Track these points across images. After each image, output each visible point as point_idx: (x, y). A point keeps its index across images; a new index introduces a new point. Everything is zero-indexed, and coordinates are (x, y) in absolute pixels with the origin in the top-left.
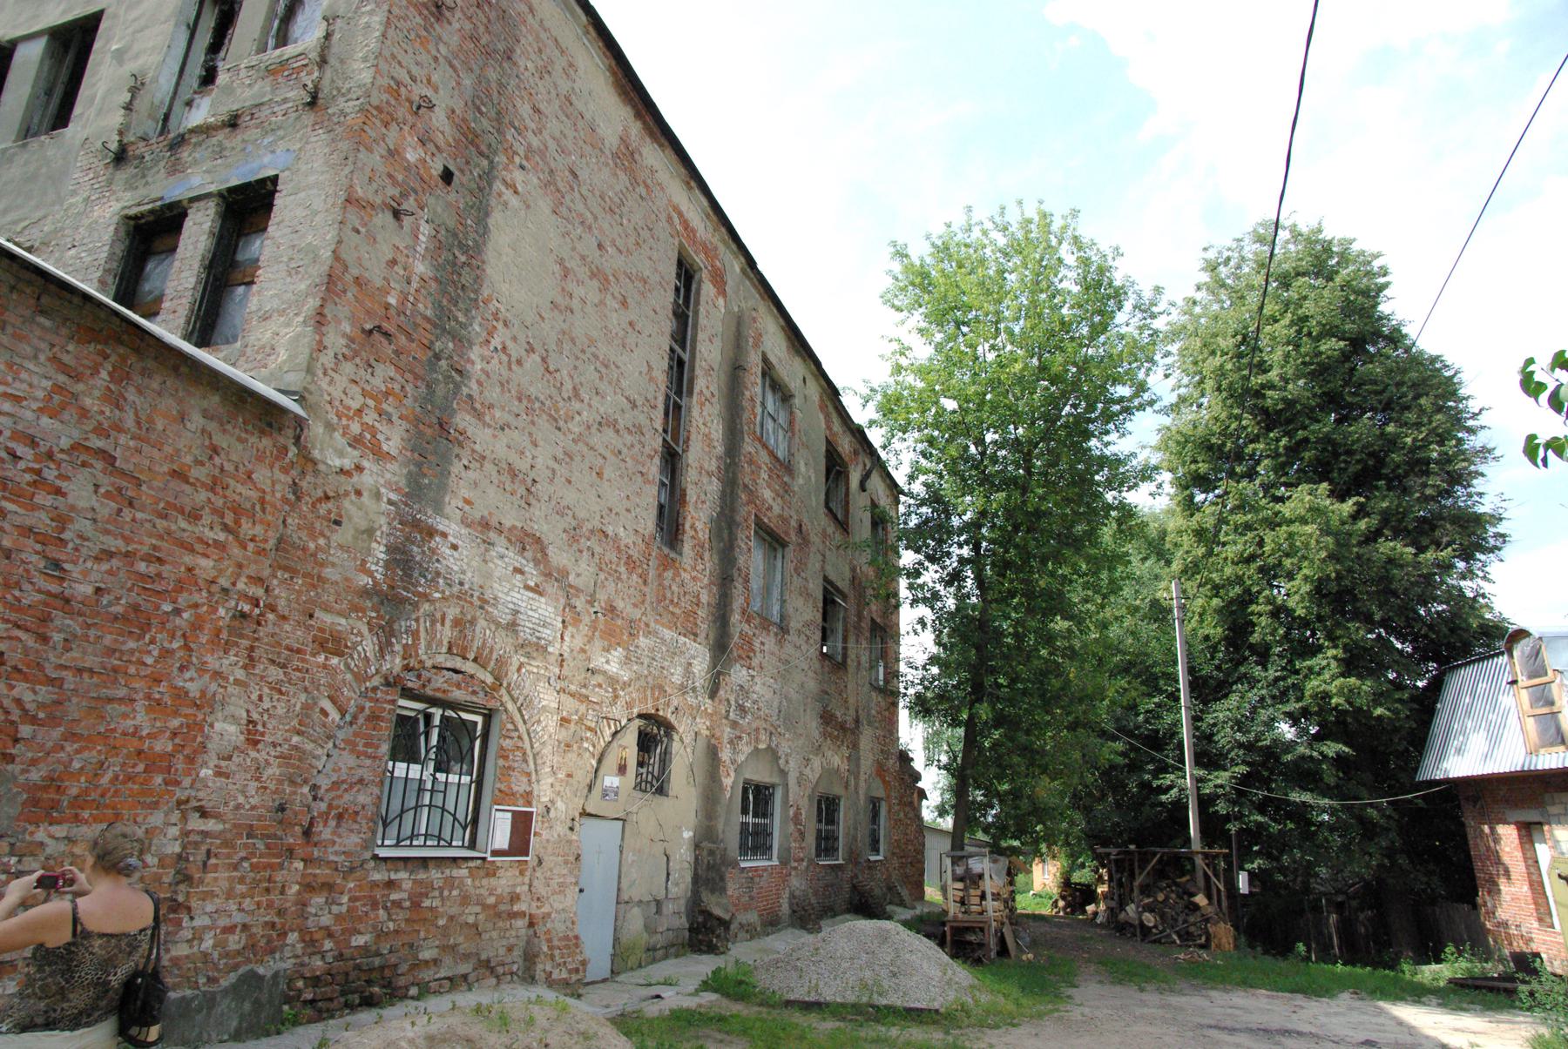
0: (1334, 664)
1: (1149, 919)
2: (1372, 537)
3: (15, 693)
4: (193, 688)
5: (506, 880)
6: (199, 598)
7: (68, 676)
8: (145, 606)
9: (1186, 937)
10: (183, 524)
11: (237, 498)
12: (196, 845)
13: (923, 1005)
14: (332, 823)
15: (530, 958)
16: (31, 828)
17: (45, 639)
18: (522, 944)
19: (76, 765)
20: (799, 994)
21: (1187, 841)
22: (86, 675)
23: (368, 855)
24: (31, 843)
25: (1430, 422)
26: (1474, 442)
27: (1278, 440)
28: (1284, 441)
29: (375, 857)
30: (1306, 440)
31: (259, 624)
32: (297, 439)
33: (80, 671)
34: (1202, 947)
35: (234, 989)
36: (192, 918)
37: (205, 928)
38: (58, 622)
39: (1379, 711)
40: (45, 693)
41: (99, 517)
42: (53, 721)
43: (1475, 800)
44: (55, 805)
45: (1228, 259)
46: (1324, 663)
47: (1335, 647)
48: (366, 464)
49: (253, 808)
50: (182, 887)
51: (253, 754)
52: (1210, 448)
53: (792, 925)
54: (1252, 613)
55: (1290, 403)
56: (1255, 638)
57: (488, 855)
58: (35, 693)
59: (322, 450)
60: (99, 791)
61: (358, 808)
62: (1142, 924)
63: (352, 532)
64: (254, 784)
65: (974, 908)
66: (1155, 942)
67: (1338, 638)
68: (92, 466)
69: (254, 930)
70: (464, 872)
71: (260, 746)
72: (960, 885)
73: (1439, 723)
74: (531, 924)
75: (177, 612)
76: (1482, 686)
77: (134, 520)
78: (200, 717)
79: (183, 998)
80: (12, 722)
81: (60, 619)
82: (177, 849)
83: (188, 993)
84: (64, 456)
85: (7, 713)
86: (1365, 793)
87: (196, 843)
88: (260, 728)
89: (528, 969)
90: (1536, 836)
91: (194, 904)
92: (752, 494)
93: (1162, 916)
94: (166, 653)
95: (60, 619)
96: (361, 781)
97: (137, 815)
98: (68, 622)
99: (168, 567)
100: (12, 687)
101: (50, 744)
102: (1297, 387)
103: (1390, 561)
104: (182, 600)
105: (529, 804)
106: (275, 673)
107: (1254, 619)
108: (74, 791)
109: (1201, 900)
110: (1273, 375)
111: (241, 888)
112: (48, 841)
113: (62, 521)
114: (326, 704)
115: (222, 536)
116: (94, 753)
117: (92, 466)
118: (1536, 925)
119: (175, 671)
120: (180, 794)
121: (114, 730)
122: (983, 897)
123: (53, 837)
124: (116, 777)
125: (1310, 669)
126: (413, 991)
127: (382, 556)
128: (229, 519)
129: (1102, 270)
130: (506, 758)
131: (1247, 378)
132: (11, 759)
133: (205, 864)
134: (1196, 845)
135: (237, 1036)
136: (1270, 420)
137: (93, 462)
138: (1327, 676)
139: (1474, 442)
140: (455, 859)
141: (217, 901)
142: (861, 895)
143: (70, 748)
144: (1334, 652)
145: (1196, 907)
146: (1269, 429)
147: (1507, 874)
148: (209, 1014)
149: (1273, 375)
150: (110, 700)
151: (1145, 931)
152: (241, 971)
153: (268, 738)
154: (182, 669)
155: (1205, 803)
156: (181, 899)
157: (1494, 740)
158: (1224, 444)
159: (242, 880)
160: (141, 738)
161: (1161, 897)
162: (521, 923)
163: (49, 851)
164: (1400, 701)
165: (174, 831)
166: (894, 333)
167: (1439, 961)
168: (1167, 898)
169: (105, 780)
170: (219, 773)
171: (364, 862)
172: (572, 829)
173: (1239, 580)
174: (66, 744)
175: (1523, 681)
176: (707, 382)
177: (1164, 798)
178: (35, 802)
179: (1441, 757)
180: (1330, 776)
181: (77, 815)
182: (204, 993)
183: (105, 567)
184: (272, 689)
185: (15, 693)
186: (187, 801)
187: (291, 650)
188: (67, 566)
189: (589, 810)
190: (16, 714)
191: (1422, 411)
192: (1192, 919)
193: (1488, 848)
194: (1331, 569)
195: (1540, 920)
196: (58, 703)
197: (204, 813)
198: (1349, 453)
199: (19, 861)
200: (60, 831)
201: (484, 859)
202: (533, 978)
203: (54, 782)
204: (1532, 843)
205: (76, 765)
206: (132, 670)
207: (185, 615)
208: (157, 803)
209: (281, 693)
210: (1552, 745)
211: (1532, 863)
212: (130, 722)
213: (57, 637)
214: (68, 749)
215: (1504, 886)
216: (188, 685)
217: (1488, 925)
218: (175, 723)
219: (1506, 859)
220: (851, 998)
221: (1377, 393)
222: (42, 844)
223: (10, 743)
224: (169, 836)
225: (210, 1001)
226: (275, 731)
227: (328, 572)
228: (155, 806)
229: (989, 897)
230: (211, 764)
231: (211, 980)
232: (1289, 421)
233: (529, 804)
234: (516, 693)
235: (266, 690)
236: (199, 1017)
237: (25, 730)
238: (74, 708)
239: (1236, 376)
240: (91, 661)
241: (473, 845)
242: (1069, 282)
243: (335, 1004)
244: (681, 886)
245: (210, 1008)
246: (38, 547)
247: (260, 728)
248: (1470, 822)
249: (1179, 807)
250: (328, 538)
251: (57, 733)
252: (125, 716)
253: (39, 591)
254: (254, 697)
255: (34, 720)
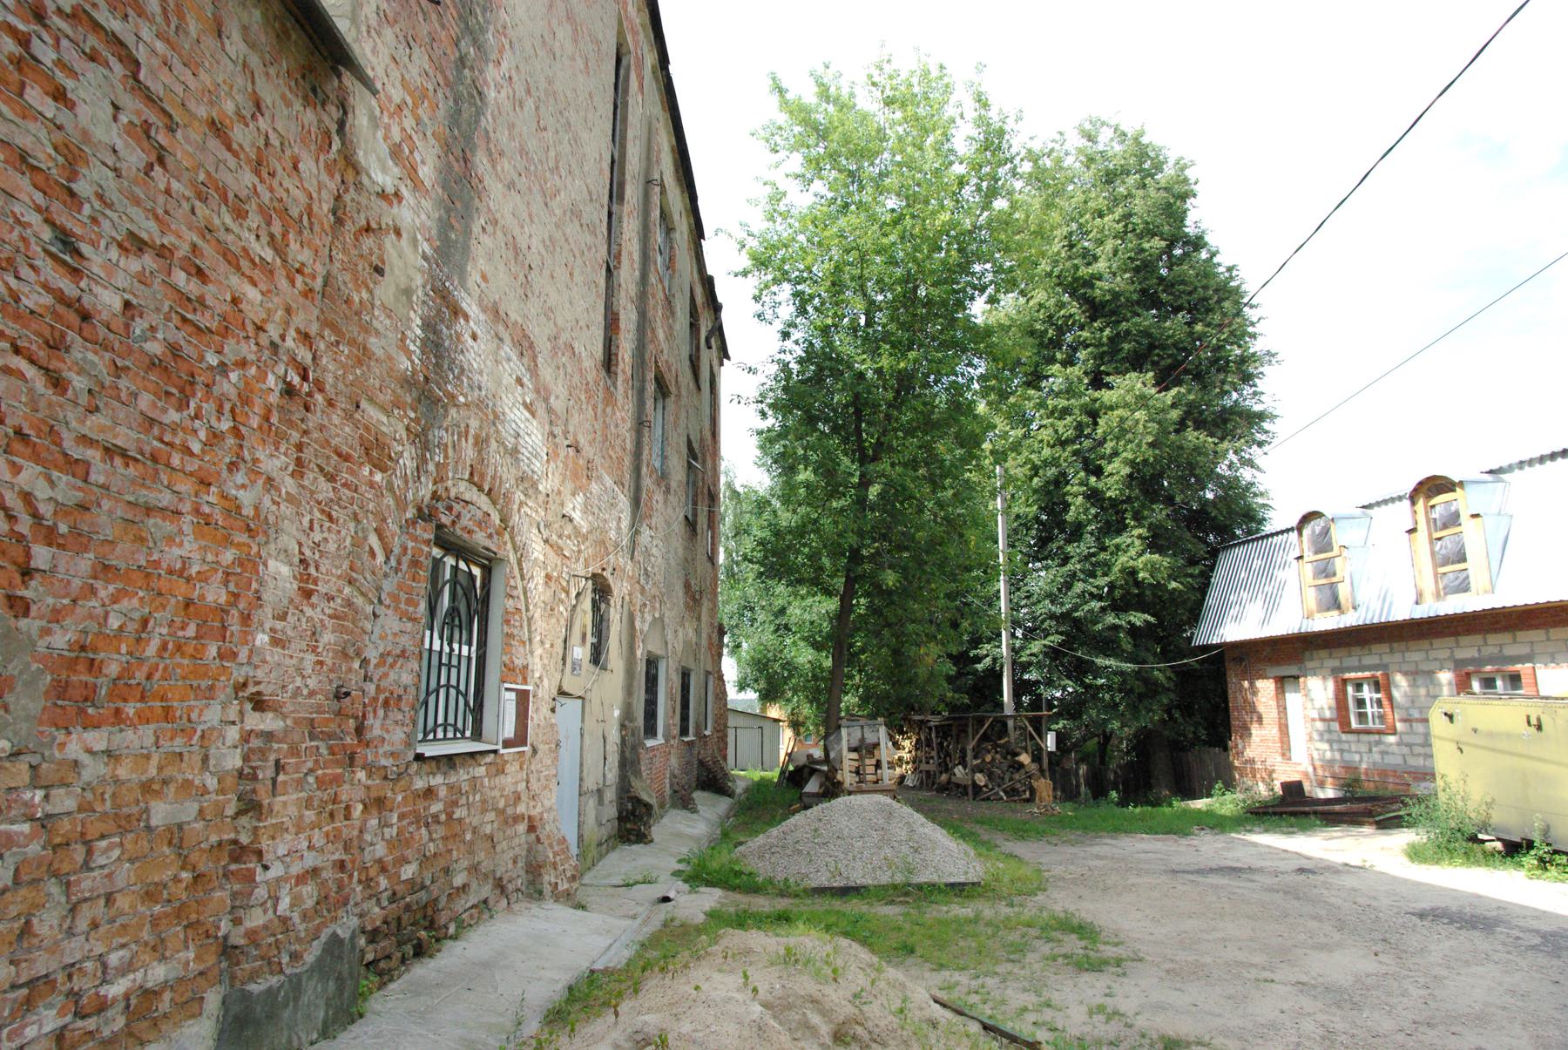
0: (1137, 542)
1: (980, 779)
2: (1181, 426)
3: (23, 479)
4: (246, 498)
5: (512, 779)
6: (248, 350)
7: (93, 455)
8: (188, 350)
9: (1012, 792)
10: (228, 220)
11: (285, 195)
12: (263, 753)
13: (962, 879)
14: (381, 713)
15: (534, 870)
16: (61, 736)
17: (58, 383)
18: (524, 853)
19: (114, 623)
20: (823, 880)
21: (1000, 705)
22: (118, 461)
23: (411, 756)
24: (62, 763)
25: (1230, 324)
26: (1257, 347)
27: (1102, 330)
28: (1107, 332)
29: (419, 757)
30: (1128, 332)
31: (307, 409)
32: (341, 125)
33: (110, 451)
34: (1028, 801)
35: (319, 967)
36: (266, 868)
37: (278, 880)
38: (76, 354)
39: (1174, 585)
40: (66, 489)
41: (123, 166)
42: (79, 541)
43: (1239, 660)
44: (90, 695)
45: (1052, 150)
46: (1129, 541)
47: (1140, 526)
48: (404, 192)
49: (312, 694)
50: (244, 820)
51: (309, 611)
52: (1032, 333)
53: (674, 806)
54: (1066, 494)
55: (1116, 295)
56: (1070, 516)
57: (499, 747)
58: (52, 484)
59: (366, 153)
60: (145, 669)
61: (401, 692)
62: (974, 784)
63: (392, 289)
64: (310, 658)
65: (869, 777)
66: (988, 799)
67: (1145, 518)
68: (107, 65)
69: (324, 875)
70: (481, 771)
71: (314, 599)
72: (854, 755)
73: (1212, 599)
74: (532, 829)
75: (223, 368)
76: (1257, 563)
77: (168, 192)
78: (255, 549)
79: (270, 989)
80: (21, 538)
81: (79, 351)
82: (239, 763)
83: (274, 980)
84: (63, 25)
85: (11, 518)
86: (1151, 659)
87: (261, 750)
88: (312, 570)
89: (532, 883)
90: (1287, 687)
91: (265, 843)
92: (653, 330)
93: (990, 776)
94: (215, 437)
95: (79, 351)
96: (403, 654)
97: (191, 709)
98: (90, 356)
99: (211, 288)
100: (16, 469)
101: (76, 583)
102: (1122, 282)
103: (1196, 449)
104: (230, 347)
105: (525, 682)
106: (324, 489)
107: (1069, 499)
108: (113, 669)
109: (1025, 758)
110: (1101, 266)
111: (310, 815)
112: (85, 758)
113: (72, 157)
114: (373, 540)
115: (268, 254)
116: (135, 601)
117: (107, 65)
118: (1279, 759)
119: (225, 473)
120: (239, 674)
121: (157, 564)
122: (878, 765)
123: (90, 752)
124: (164, 647)
125: (1117, 547)
126: (452, 930)
127: (418, 332)
128: (277, 228)
129: (1001, 133)
130: (507, 622)
131: (1076, 268)
132: (20, 607)
133: (274, 781)
134: (1009, 709)
135: (325, 1034)
136: (1095, 309)
137: (113, 61)
138: (1133, 552)
139: (1257, 347)
140: (472, 755)
141: (288, 837)
142: (709, 770)
143: (105, 591)
144: (1141, 531)
145: (1021, 765)
146: (1093, 319)
147: (1260, 720)
148: (296, 1007)
149: (1101, 266)
150: (149, 510)
151: (977, 789)
152: (324, 938)
153: (322, 588)
154: (232, 467)
155: (1019, 667)
156: (244, 839)
157: (1271, 605)
158: (1046, 331)
159: (308, 803)
160: (188, 580)
161: (988, 758)
162: (522, 828)
163: (87, 775)
164: (1191, 576)
165: (233, 733)
166: (769, 177)
167: (1209, 795)
168: (993, 759)
169: (151, 650)
170: (276, 642)
171: (408, 765)
172: (553, 710)
173: (1054, 462)
174: (98, 584)
175: (1309, 556)
176: (632, 192)
177: (979, 667)
178: (61, 689)
179: (1219, 622)
180: (1126, 643)
181: (118, 711)
182: (290, 977)
183: (134, 265)
184: (322, 512)
185: (23, 479)
186: (245, 685)
187: (339, 455)
188: (86, 249)
189: (566, 688)
190: (25, 525)
191: (1224, 315)
192: (1017, 776)
193: (1246, 701)
194: (1150, 454)
195: (1283, 755)
196: (83, 507)
197: (259, 704)
198: (1163, 347)
199: (46, 797)
200: (98, 739)
201: (495, 752)
202: (541, 893)
203: (85, 654)
204: (1283, 693)
205: (114, 623)
206: (176, 460)
207: (234, 376)
208: (211, 688)
209: (330, 517)
210: (1328, 609)
211: (1282, 709)
212: (177, 552)
213: (79, 383)
214: (102, 593)
215: (1255, 730)
216: (241, 494)
217: (1236, 763)
218: (228, 556)
219: (1261, 708)
220: (885, 879)
221: (1190, 293)
222: (76, 763)
223: (18, 579)
224: (229, 742)
225: (296, 984)
226: (329, 579)
227: (373, 342)
228: (209, 694)
229: (885, 765)
230: (267, 626)
231: (295, 956)
232: (1113, 313)
233: (525, 682)
234: (518, 539)
235: (317, 514)
236: (286, 1014)
237: (42, 555)
238: (106, 519)
239: (1068, 264)
240: (125, 437)
241: (477, 735)
242: (964, 140)
243: (394, 962)
244: (612, 776)
245: (296, 999)
246: (39, 197)
247: (312, 570)
248: (1232, 679)
249: (994, 675)
250: (371, 292)
251: (85, 563)
252: (170, 540)
253: (46, 286)
254: (306, 521)
255: (50, 537)
